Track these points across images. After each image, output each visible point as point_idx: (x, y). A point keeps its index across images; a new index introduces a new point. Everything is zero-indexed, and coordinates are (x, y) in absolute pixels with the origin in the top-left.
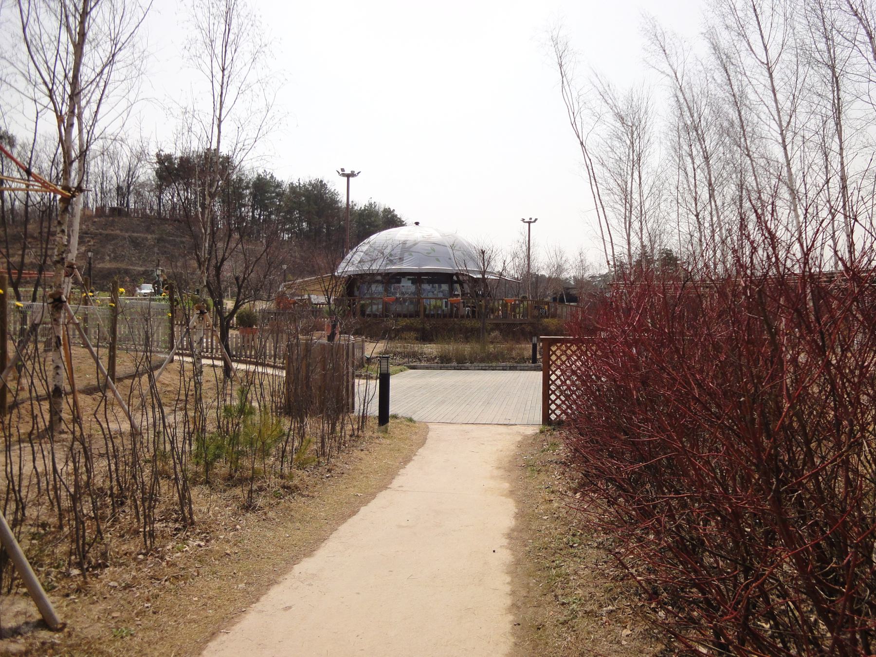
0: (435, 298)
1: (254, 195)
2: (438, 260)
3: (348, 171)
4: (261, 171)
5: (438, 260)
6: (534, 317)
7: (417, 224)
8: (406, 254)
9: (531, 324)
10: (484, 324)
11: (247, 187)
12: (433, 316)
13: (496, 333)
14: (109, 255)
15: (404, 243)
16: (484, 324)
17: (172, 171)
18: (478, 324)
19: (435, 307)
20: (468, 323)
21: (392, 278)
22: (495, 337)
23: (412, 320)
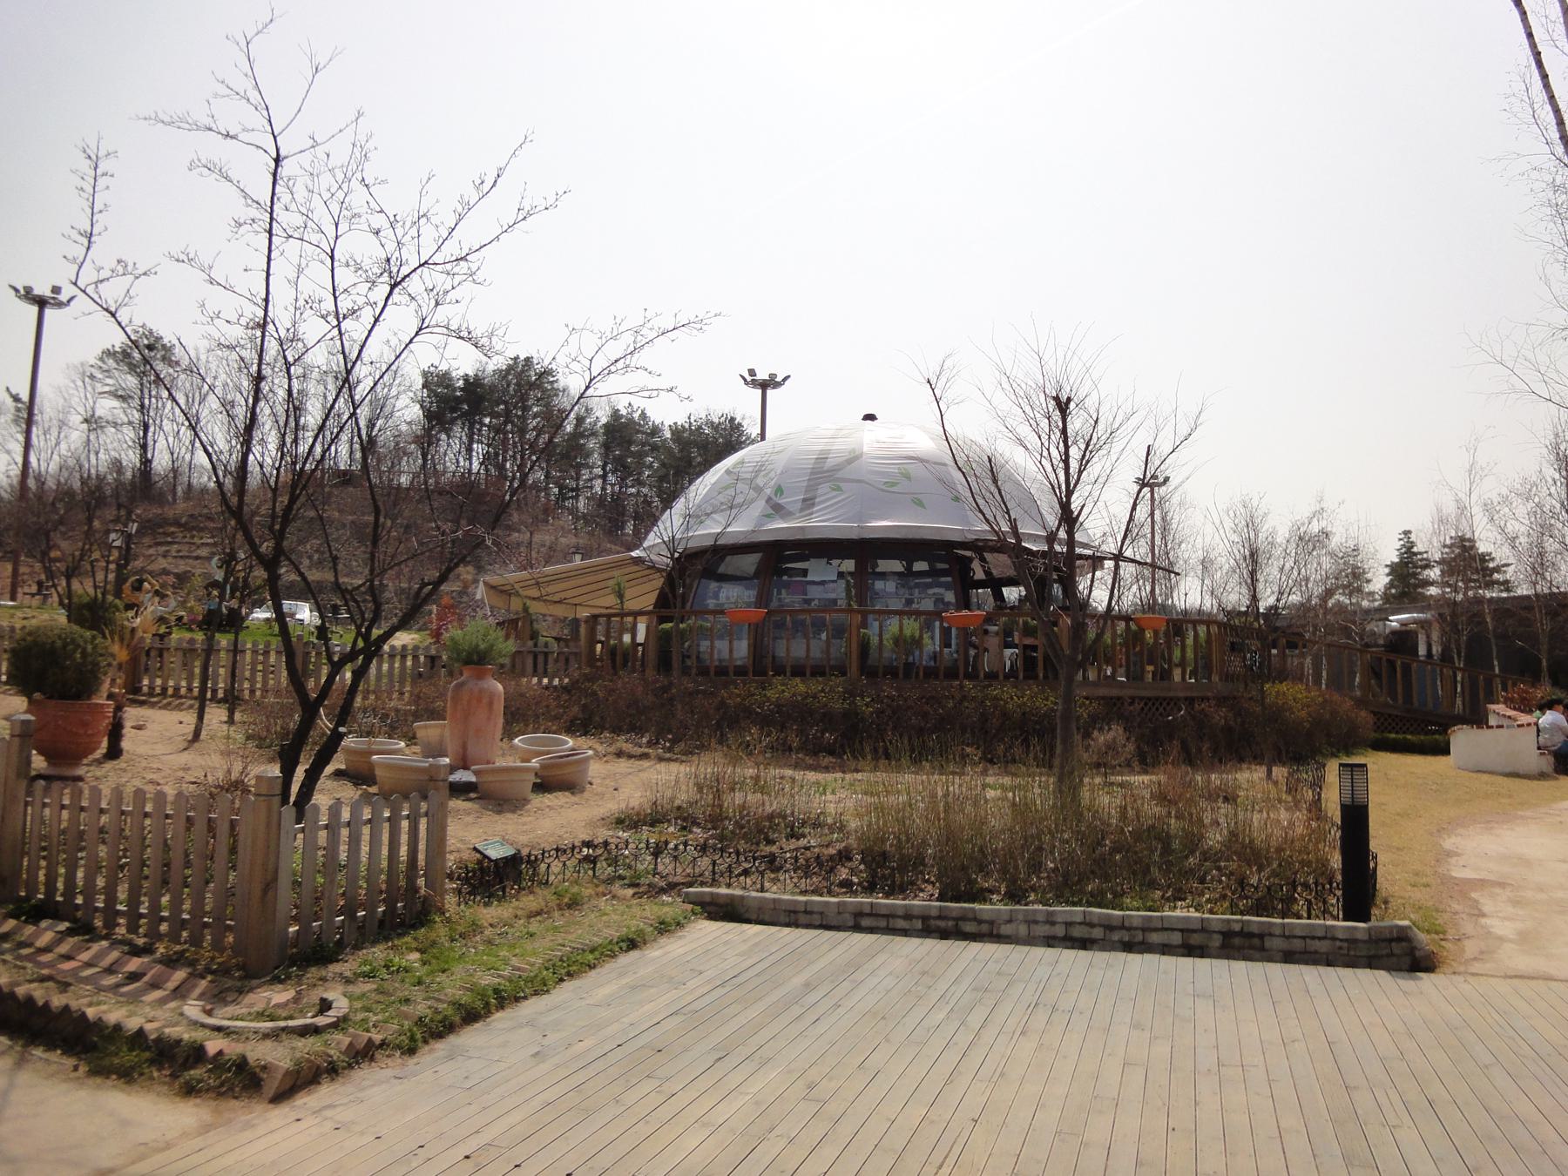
0: (901, 620)
1: (607, 447)
2: (920, 504)
3: (762, 375)
4: (622, 406)
5: (920, 504)
6: (1228, 677)
7: (870, 417)
8: (824, 489)
9: (1222, 700)
10: (1068, 699)
11: (594, 434)
12: (891, 672)
13: (1111, 734)
14: (310, 557)
15: (822, 458)
16: (1068, 699)
17: (453, 403)
18: (1043, 700)
19: (898, 640)
20: (1014, 697)
21: (778, 558)
22: (1111, 747)
23: (815, 685)
